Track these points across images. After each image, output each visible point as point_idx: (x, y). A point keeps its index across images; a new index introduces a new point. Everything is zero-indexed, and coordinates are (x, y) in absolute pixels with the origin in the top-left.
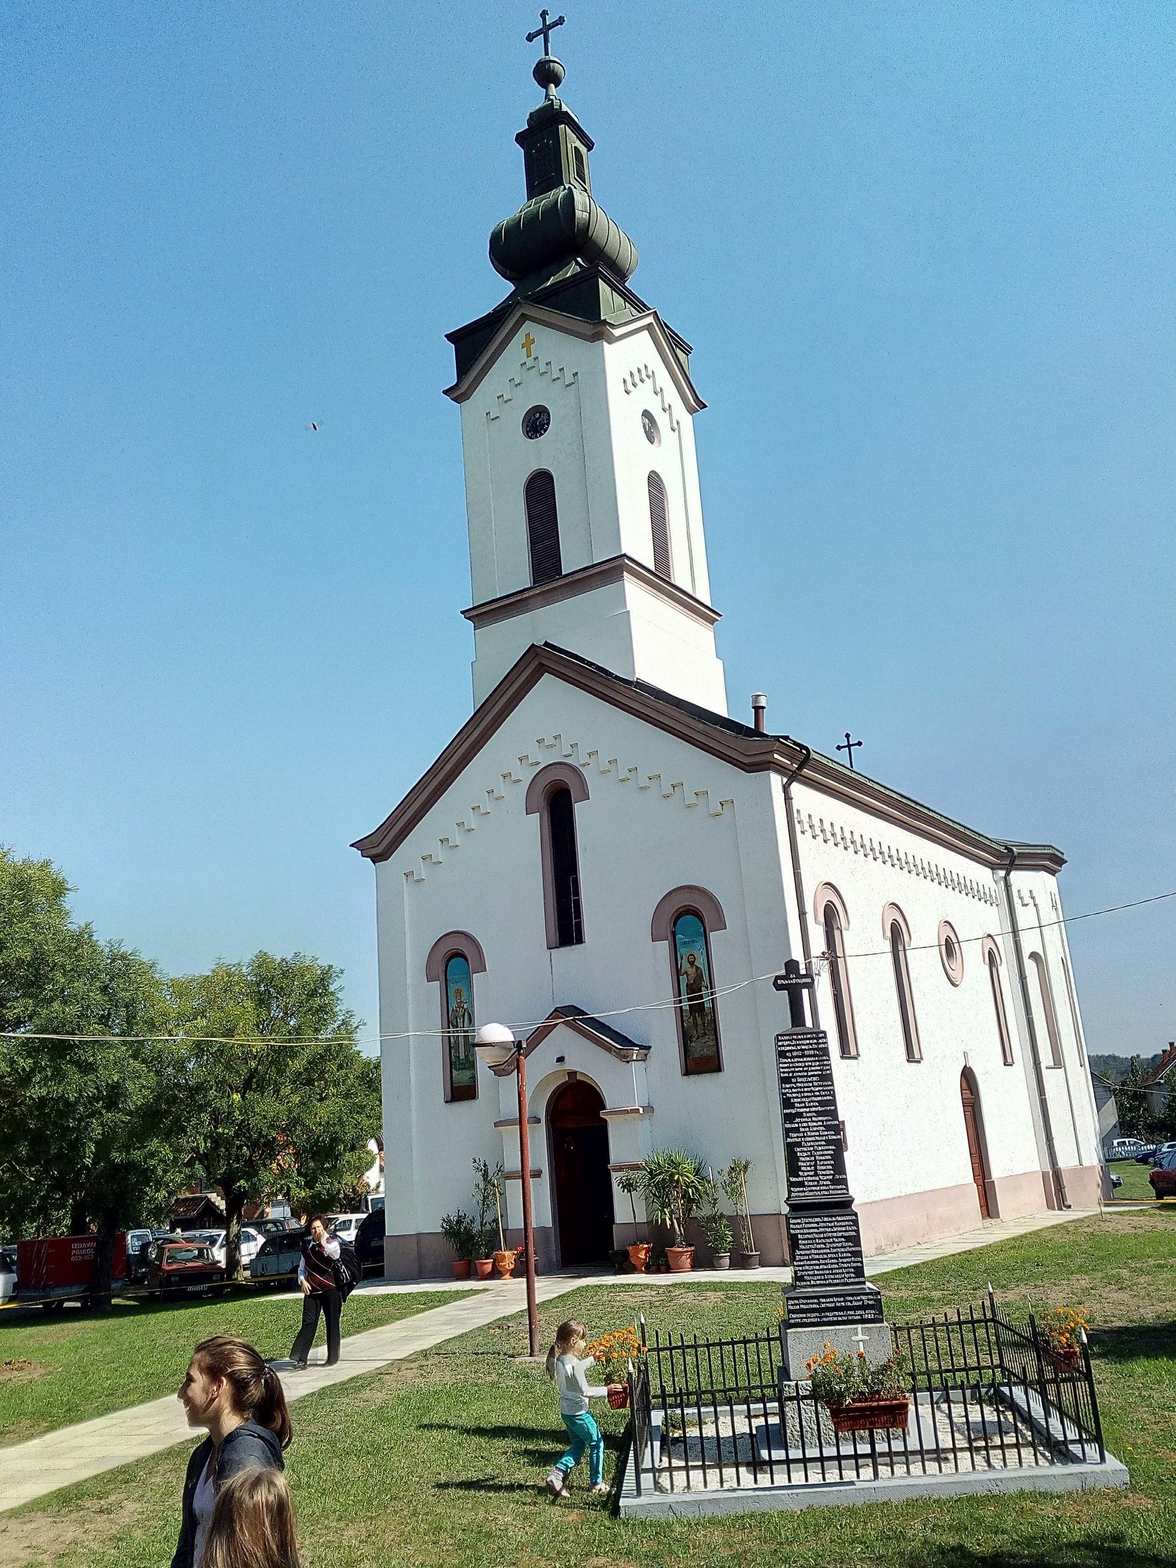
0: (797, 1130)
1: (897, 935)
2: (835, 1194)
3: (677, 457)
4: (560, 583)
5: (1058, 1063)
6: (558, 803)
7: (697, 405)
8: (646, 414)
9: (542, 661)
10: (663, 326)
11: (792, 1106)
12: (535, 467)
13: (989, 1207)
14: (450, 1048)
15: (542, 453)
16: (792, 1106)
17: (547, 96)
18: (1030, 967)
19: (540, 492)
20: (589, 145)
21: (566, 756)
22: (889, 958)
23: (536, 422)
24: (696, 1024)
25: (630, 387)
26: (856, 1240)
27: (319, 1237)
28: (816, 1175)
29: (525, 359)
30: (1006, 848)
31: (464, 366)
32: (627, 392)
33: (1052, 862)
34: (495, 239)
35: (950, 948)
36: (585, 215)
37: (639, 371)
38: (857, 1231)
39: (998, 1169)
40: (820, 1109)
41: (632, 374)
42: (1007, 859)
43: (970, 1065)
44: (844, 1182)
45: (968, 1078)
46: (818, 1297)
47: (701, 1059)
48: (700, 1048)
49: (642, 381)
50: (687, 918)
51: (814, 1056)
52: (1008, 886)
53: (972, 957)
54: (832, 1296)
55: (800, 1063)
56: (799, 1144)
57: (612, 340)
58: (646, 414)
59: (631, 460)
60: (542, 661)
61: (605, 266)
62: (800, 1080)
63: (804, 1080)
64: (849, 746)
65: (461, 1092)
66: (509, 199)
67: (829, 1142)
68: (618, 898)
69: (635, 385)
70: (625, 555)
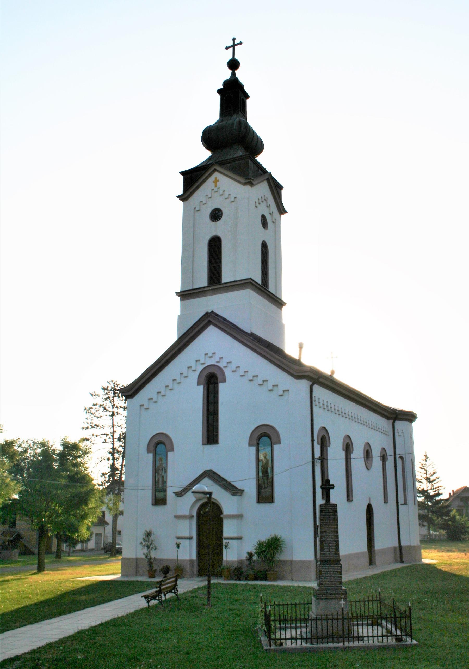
1: (348, 448)
5: (405, 504)
6: (211, 381)
9: (210, 319)
13: (371, 562)
14: (155, 482)
21: (217, 362)
22: (344, 461)
23: (216, 215)
24: (264, 482)
25: (257, 205)
29: (213, 187)
32: (256, 207)
35: (368, 454)
39: (378, 545)
45: (369, 510)
47: (265, 494)
48: (265, 492)
52: (394, 427)
60: (210, 319)
65: (159, 501)
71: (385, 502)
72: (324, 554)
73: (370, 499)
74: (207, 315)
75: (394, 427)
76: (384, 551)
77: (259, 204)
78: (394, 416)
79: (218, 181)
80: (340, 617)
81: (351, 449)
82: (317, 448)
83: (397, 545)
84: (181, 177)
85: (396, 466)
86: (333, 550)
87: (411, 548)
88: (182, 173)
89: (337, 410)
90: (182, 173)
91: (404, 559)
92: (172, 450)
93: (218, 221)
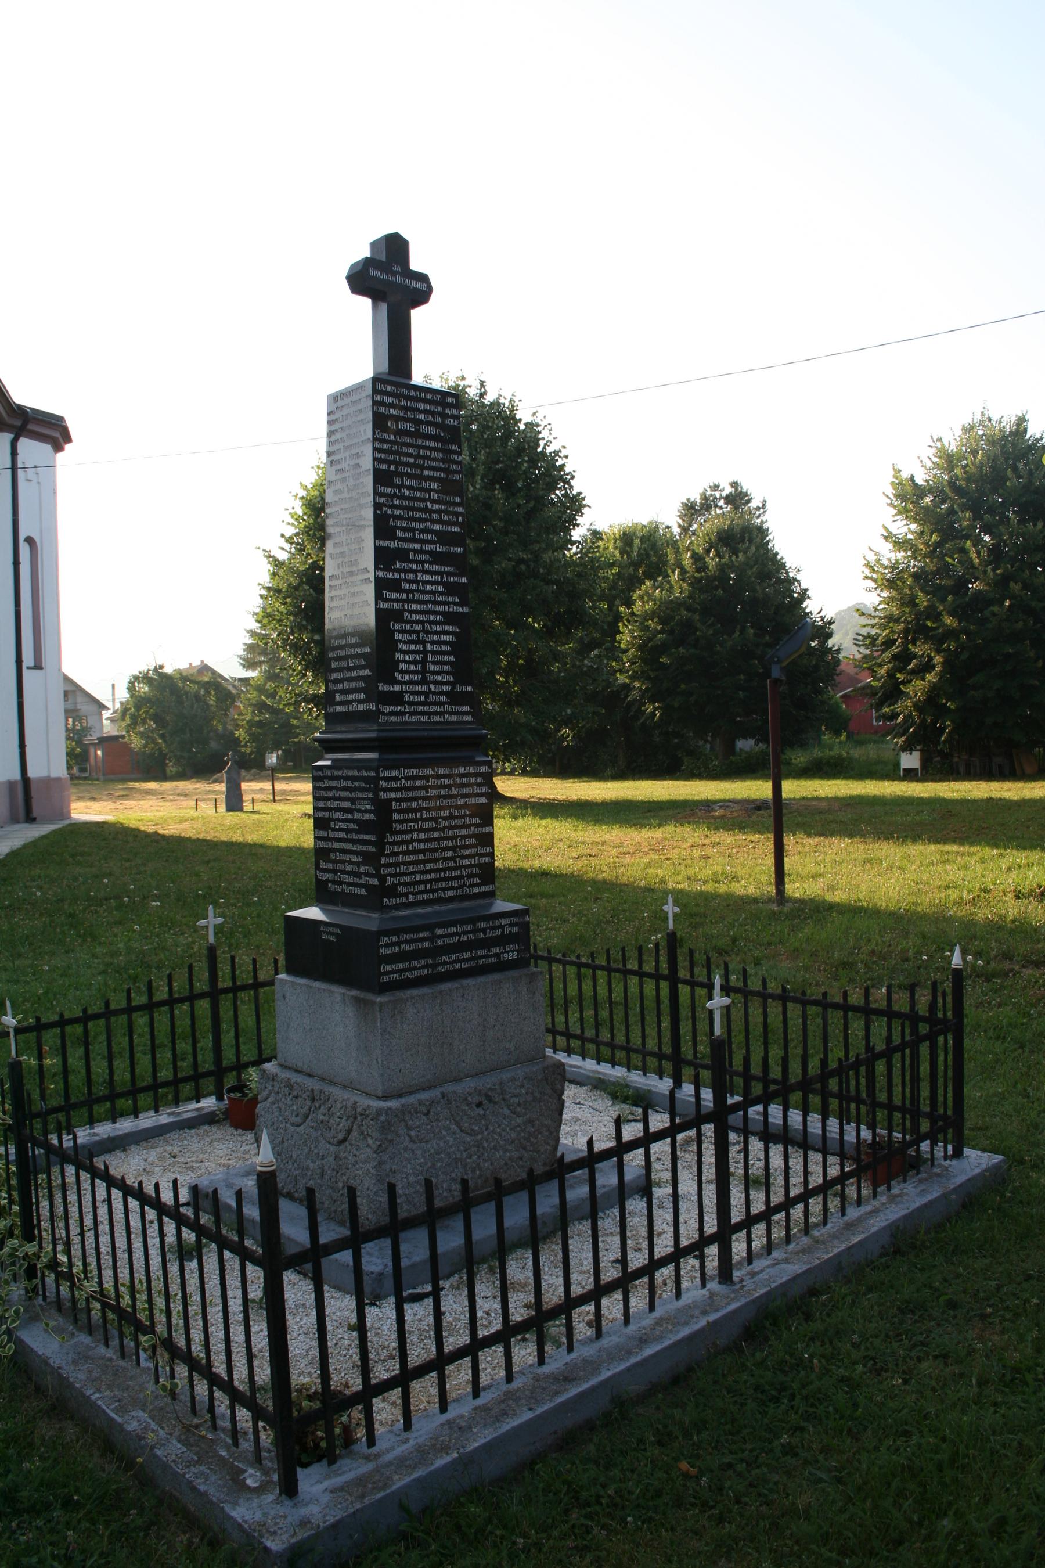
5: (38, 666)
27: (666, 613)
28: (424, 681)
46: (430, 928)
52: (14, 453)
54: (454, 923)
62: (407, 482)
78: (18, 423)
83: (17, 776)
85: (16, 563)
87: (49, 782)
91: (35, 813)
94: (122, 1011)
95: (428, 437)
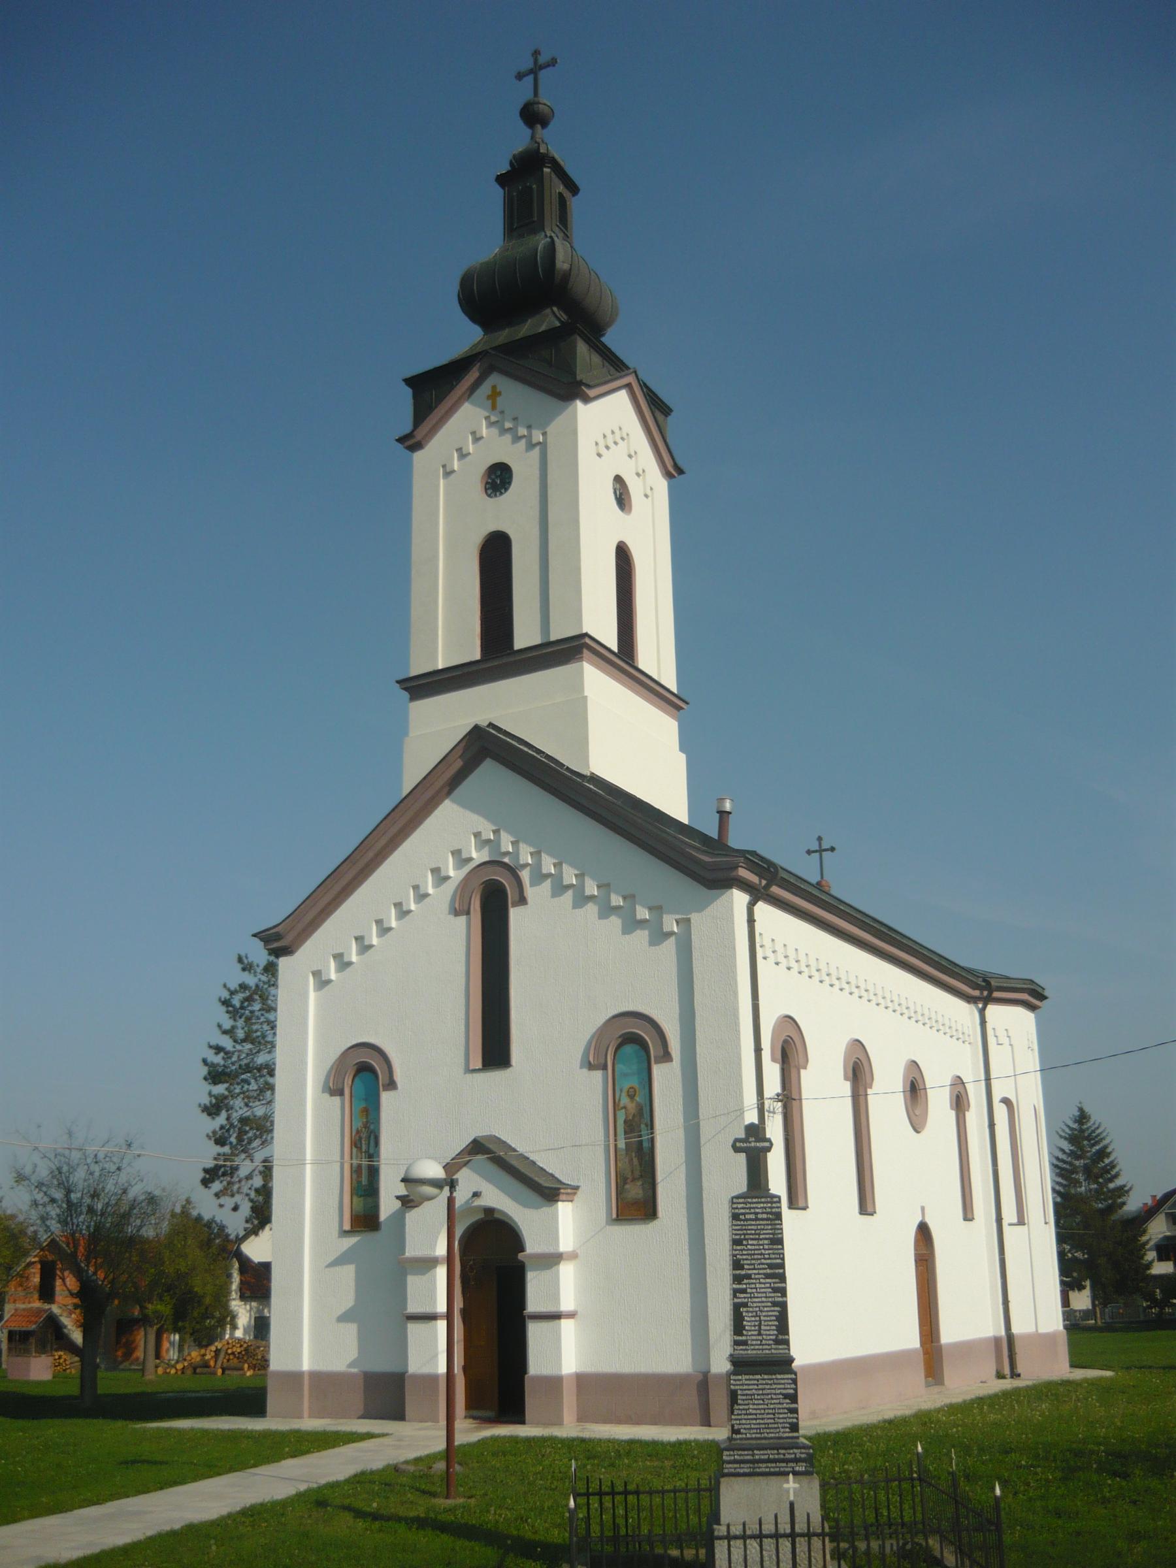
0: (744, 1291)
1: (858, 1072)
2: (779, 1350)
3: (650, 533)
4: (512, 659)
5: (1021, 1222)
6: (492, 902)
7: (673, 471)
8: (618, 479)
9: (484, 746)
10: (644, 386)
11: (742, 1268)
12: (492, 528)
15: (512, 514)
16: (742, 1268)
17: (533, 137)
18: (1001, 1112)
19: (496, 555)
20: (574, 189)
22: (848, 1102)
23: (498, 478)
25: (603, 450)
26: (794, 1398)
28: (760, 1334)
30: (984, 980)
31: (419, 417)
32: (599, 455)
33: (1031, 995)
34: (466, 282)
35: (915, 1090)
36: (566, 266)
37: (613, 432)
38: (796, 1390)
40: (768, 1271)
41: (605, 436)
42: (982, 989)
43: (928, 1220)
44: (787, 1342)
45: (924, 1233)
49: (616, 443)
50: (630, 1046)
51: (767, 1219)
52: (983, 1022)
53: (939, 1102)
55: (752, 1226)
56: (745, 1305)
57: (587, 400)
58: (618, 479)
59: (598, 528)
60: (484, 746)
61: (587, 323)
63: (755, 1242)
64: (821, 851)
66: (484, 239)
67: (775, 1304)
68: (555, 1010)
69: (607, 448)
70: (586, 635)
71: (966, 1219)
72: (745, 1343)
73: (923, 1209)
74: (476, 733)
75: (983, 1022)
76: (966, 1349)
77: (607, 448)
79: (500, 394)
80: (785, 1528)
81: (868, 1075)
82: (773, 1072)
84: (408, 392)
85: (992, 1126)
86: (770, 1331)
88: (411, 382)
89: (834, 978)
90: (411, 382)
92: (391, 1085)
93: (501, 494)
94: (695, 1490)
95: (763, 1219)
